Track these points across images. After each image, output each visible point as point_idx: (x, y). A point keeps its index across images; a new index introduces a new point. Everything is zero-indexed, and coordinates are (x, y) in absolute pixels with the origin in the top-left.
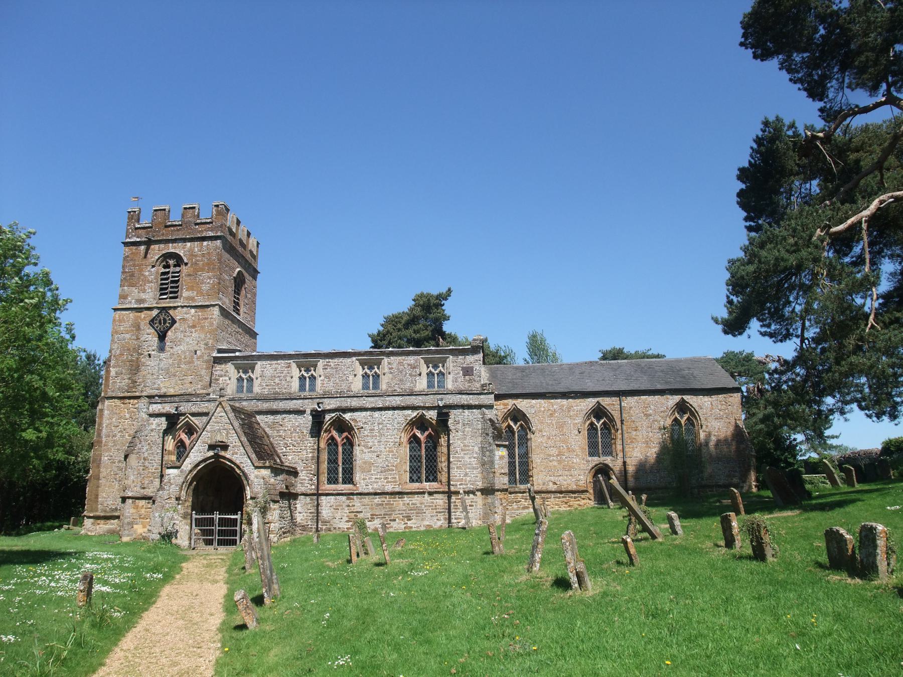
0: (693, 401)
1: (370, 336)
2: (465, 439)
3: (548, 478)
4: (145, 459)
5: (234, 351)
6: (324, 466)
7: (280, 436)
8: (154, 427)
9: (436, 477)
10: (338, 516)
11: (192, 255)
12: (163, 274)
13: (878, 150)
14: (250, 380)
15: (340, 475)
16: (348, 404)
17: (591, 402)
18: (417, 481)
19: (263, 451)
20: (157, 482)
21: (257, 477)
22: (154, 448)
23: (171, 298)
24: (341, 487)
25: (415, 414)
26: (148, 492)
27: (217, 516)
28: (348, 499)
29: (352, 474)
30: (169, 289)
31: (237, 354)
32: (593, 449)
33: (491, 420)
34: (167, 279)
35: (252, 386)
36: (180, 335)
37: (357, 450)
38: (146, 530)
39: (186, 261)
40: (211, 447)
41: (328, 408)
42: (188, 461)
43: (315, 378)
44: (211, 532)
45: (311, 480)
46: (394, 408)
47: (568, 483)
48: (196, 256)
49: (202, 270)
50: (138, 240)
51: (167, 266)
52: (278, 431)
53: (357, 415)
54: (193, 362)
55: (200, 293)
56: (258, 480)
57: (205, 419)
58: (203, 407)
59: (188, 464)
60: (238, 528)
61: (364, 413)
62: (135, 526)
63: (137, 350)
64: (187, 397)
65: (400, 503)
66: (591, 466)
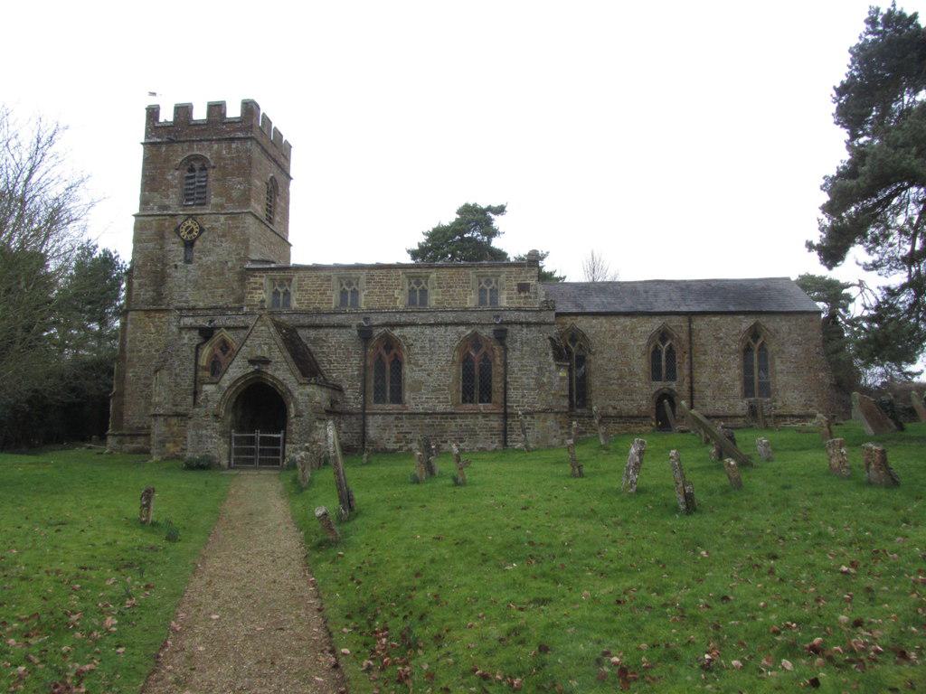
0: (769, 324)
1: (408, 251)
2: (523, 358)
3: (608, 402)
4: (176, 375)
5: (268, 262)
6: (371, 384)
7: (323, 352)
8: (186, 341)
9: (490, 398)
10: (386, 436)
11: (219, 157)
12: (188, 178)
13: (234, 146)
14: (287, 294)
15: (388, 394)
16: (403, 319)
17: (657, 323)
18: (470, 402)
19: (308, 367)
20: (190, 399)
21: (301, 394)
22: (187, 364)
23: (198, 205)
24: (389, 407)
25: (469, 332)
26: (181, 409)
27: (258, 435)
28: (396, 418)
29: (401, 393)
30: (196, 195)
31: (273, 265)
32: (656, 374)
33: (550, 338)
34: (192, 184)
35: (289, 300)
36: (209, 245)
37: (407, 369)
38: (178, 449)
39: (212, 164)
40: (252, 362)
41: (376, 323)
42: (226, 377)
43: (357, 292)
44: (252, 452)
45: (357, 398)
46: (447, 325)
47: (627, 406)
48: (224, 159)
49: (233, 175)
50: (159, 140)
51: (192, 170)
52: (321, 347)
53: (407, 330)
54: (223, 274)
55: (230, 199)
56: (303, 396)
57: (242, 334)
58: (240, 320)
59: (226, 380)
60: (281, 448)
61: (414, 329)
62: (168, 445)
63: (162, 260)
64: (222, 310)
65: (452, 425)
66: (654, 390)
